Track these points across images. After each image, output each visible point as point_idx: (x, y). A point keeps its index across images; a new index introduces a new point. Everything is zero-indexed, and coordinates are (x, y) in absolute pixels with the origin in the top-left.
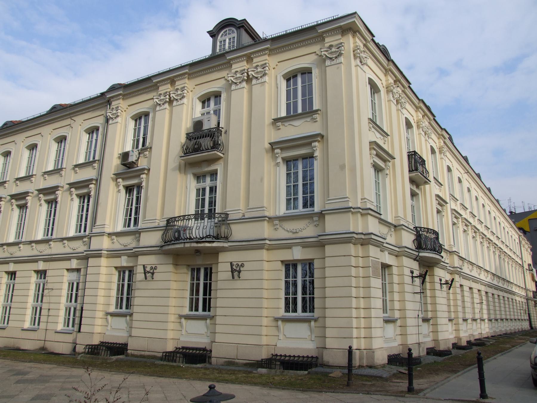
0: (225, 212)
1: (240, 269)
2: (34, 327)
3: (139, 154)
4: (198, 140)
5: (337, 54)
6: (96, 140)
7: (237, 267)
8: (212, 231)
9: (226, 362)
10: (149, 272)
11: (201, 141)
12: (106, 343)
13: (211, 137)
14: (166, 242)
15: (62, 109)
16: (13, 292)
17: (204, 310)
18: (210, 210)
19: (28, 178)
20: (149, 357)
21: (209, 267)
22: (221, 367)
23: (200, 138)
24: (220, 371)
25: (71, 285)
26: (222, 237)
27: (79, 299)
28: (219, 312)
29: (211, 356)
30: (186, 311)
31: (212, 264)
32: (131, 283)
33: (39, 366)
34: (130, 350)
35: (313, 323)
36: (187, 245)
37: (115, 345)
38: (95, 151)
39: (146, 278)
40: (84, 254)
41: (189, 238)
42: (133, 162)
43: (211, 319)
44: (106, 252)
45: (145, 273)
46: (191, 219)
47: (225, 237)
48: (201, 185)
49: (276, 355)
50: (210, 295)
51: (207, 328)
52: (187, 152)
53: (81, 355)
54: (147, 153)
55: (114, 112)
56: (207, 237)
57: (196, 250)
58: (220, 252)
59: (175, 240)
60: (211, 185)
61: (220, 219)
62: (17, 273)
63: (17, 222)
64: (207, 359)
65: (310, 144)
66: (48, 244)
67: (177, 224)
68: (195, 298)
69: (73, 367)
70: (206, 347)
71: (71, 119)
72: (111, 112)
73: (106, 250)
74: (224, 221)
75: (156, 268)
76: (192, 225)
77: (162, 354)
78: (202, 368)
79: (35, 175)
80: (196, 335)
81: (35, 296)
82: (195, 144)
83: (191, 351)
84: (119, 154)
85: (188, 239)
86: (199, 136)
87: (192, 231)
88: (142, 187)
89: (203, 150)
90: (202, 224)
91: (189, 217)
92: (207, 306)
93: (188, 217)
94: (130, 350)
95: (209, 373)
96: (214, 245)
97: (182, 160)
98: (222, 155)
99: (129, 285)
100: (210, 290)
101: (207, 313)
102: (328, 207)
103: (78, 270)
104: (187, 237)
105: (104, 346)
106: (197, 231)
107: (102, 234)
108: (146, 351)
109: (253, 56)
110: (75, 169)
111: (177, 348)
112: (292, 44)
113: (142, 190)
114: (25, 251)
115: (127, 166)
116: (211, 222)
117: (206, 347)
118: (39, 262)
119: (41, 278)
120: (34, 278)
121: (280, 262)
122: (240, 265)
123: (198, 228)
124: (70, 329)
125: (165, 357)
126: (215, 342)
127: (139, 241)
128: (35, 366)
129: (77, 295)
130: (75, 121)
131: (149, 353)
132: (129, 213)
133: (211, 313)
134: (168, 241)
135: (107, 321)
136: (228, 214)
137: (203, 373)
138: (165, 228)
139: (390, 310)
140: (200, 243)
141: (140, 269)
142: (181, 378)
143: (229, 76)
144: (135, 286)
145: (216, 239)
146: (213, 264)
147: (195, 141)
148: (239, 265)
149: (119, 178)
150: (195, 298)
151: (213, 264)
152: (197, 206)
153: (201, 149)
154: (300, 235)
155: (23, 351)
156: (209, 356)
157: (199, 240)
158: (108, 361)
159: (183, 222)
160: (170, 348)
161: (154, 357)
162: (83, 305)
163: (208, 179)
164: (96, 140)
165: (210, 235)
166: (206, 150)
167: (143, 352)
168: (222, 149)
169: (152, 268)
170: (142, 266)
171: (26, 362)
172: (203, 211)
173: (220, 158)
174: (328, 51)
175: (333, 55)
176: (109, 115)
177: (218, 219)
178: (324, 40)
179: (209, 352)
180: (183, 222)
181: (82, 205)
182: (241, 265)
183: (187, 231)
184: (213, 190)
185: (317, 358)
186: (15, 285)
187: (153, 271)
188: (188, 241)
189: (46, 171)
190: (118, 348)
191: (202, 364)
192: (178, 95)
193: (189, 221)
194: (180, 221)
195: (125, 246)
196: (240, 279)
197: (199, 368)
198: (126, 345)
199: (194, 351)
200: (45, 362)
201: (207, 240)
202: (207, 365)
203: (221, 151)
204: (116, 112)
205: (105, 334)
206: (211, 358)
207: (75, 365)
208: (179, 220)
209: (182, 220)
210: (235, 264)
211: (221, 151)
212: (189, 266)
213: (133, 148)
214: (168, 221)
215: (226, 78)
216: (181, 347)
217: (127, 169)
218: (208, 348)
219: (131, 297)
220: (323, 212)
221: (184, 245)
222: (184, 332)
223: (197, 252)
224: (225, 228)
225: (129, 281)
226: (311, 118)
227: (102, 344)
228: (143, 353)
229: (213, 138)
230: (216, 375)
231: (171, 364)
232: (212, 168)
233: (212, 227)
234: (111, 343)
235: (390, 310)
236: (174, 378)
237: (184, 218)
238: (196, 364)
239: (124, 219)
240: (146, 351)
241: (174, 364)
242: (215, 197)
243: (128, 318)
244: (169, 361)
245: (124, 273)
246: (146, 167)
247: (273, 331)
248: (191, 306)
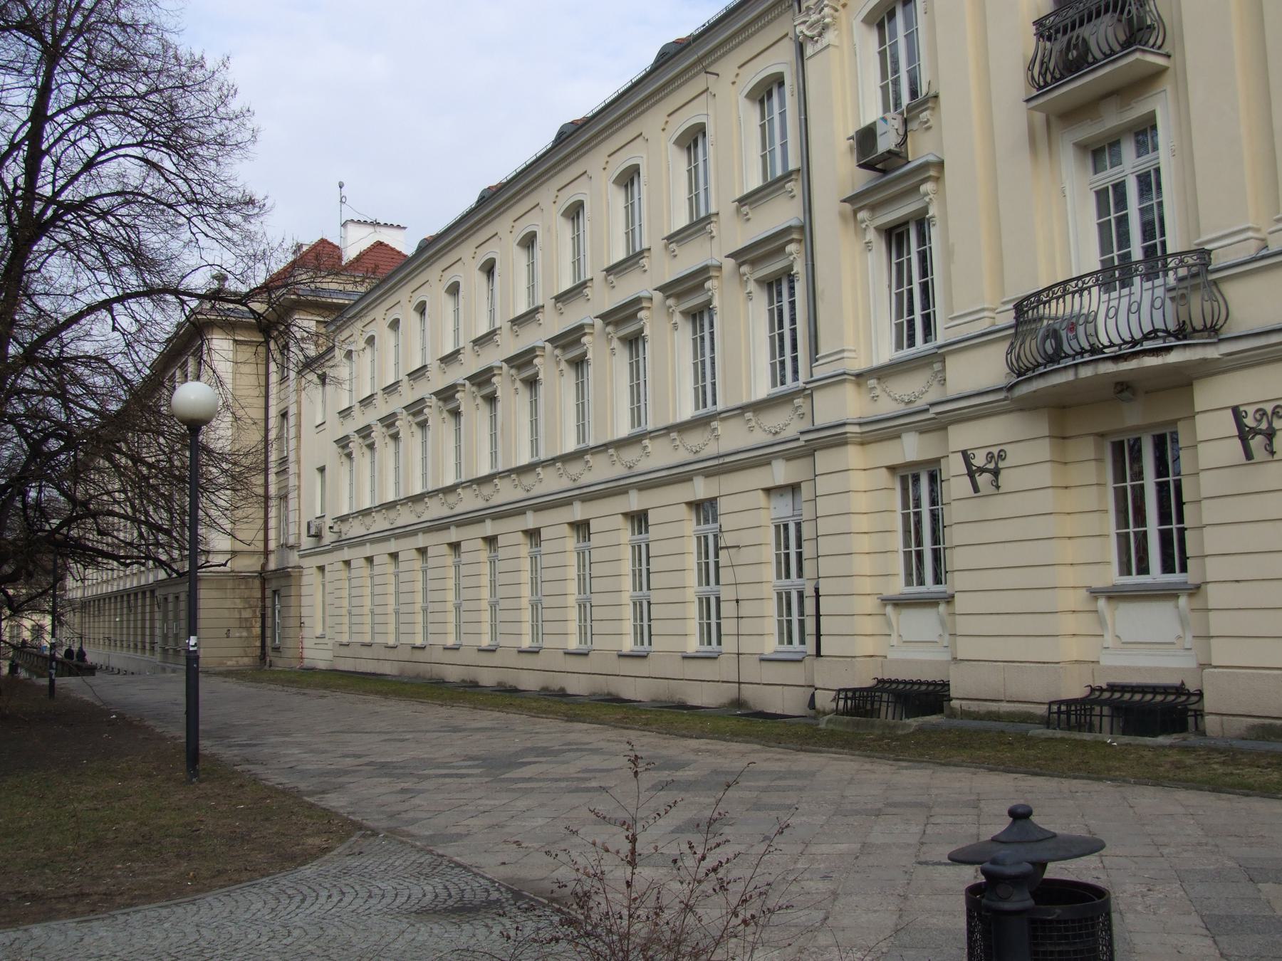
0: (1199, 244)
1: (1270, 423)
2: (709, 648)
3: (906, 122)
4: (1075, 34)
6: (783, 114)
7: (1260, 421)
8: (1158, 315)
9: (1253, 727)
10: (982, 470)
11: (1086, 31)
12: (891, 682)
13: (1115, 11)
14: (1022, 372)
15: (578, 129)
16: (648, 563)
17: (1167, 567)
18: (1149, 252)
19: (634, 259)
20: (1011, 717)
21: (1167, 431)
22: (1236, 744)
23: (1081, 24)
24: (1231, 754)
25: (781, 529)
26: (1195, 330)
27: (807, 565)
28: (1214, 569)
29: (1203, 710)
30: (1112, 576)
31: (1175, 422)
32: (940, 507)
33: (718, 747)
34: (958, 699)
36: (1085, 372)
37: (916, 687)
38: (784, 146)
39: (976, 489)
40: (801, 443)
41: (1088, 347)
42: (889, 152)
43: (1191, 595)
44: (857, 429)
45: (971, 475)
46: (1086, 289)
47: (1205, 329)
48: (1108, 177)
50: (1181, 519)
51: (1183, 622)
52: (1045, 81)
53: (827, 717)
54: (925, 115)
55: (814, 17)
56: (1146, 337)
57: (1117, 384)
58: (1197, 378)
59: (1048, 362)
60: (1143, 168)
61: (1182, 272)
62: (651, 514)
63: (629, 384)
64: (1191, 720)
66: (709, 429)
67: (1047, 311)
68: (1135, 533)
69: (801, 750)
70: (1183, 684)
71: (707, 72)
72: (804, 22)
73: (856, 421)
75: (1002, 456)
76: (1094, 307)
77: (1046, 706)
78: (1171, 747)
79: (718, 214)
80: (1151, 646)
81: (700, 570)
82: (1068, 48)
83: (1137, 697)
84: (849, 139)
85: (1087, 351)
86: (1077, 17)
87: (1096, 327)
88: (928, 219)
89: (1096, 61)
90: (1122, 300)
91: (1080, 284)
92: (1174, 556)
93: (1077, 285)
94: (958, 699)
95: (1193, 762)
96: (1173, 358)
97: (1034, 108)
98: (1161, 61)
99: (935, 517)
100: (1180, 504)
101: (1176, 577)
103: (794, 488)
104: (1082, 348)
105: (1102, 703)
106: (1111, 323)
107: (837, 380)
108: (1001, 701)
110: (742, 209)
111: (1093, 690)
113: (933, 230)
114: (659, 456)
115: (877, 166)
116: (1153, 288)
117: (1183, 684)
118: (695, 478)
119: (706, 521)
120: (690, 526)
121: (884, 470)
122: (1269, 412)
123: (1134, 308)
124: (798, 650)
125: (1059, 717)
127: (943, 381)
128: (709, 747)
129: (800, 555)
130: (718, 75)
131: (1012, 705)
132: (903, 304)
133: (1191, 577)
134: (1028, 369)
135: (889, 624)
136: (1209, 252)
137: (1172, 763)
138: (1012, 331)
139: (1109, 563)
140: (1126, 360)
141: (955, 466)
142: (1099, 779)
143: (796, 23)
144: (952, 514)
145: (1179, 339)
146: (1179, 420)
147: (1066, 37)
149: (861, 209)
150: (1135, 533)
151: (1179, 420)
152: (1105, 246)
153: (1090, 59)
155: (691, 712)
156: (1195, 711)
158: (900, 732)
159: (1064, 301)
160: (1075, 689)
161: (1027, 718)
162: (818, 583)
163: (1128, 150)
164: (783, 114)
165: (1155, 331)
166: (1106, 56)
167: (994, 704)
168: (1159, 42)
169: (993, 457)
170: (1230, 412)
171: (691, 737)
172: (1126, 257)
173: (1159, 72)
176: (802, 32)
177: (1176, 273)
179: (1194, 699)
180: (1064, 301)
181: (897, 264)
182: (1273, 413)
183: (1081, 329)
184: (1149, 183)
186: (651, 544)
187: (997, 464)
188: (1087, 358)
189: (745, 192)
190: (927, 694)
191: (1175, 736)
192: (811, 26)
193: (1081, 296)
194: (1054, 303)
195: (907, 403)
196: (1001, 491)
197: (1163, 747)
198: (946, 685)
199: (1149, 697)
200: (735, 736)
201: (1148, 345)
202: (1192, 739)
203: (1160, 48)
204: (819, 16)
206: (1202, 716)
207: (808, 744)
208: (1052, 299)
209: (1058, 298)
210: (1251, 410)
211: (1158, 49)
212: (1102, 435)
213: (886, 109)
214: (1019, 308)
216: (1104, 686)
217: (881, 177)
218: (1191, 686)
219: (945, 549)
221: (1076, 374)
222: (1109, 640)
223: (1122, 391)
224: (1203, 299)
225: (934, 502)
227: (880, 686)
228: (993, 707)
229: (1122, 12)
230: (1214, 769)
231: (1076, 735)
232: (1137, 111)
233: (1158, 303)
234: (905, 682)
235: (1109, 563)
236: (1075, 778)
237: (1064, 290)
238: (1155, 736)
239: (893, 326)
240: (1001, 701)
241: (1087, 736)
242: (1160, 204)
243: (942, 608)
244: (1069, 728)
245: (916, 479)
246: (931, 158)
247: (1084, 623)
248: (1125, 560)
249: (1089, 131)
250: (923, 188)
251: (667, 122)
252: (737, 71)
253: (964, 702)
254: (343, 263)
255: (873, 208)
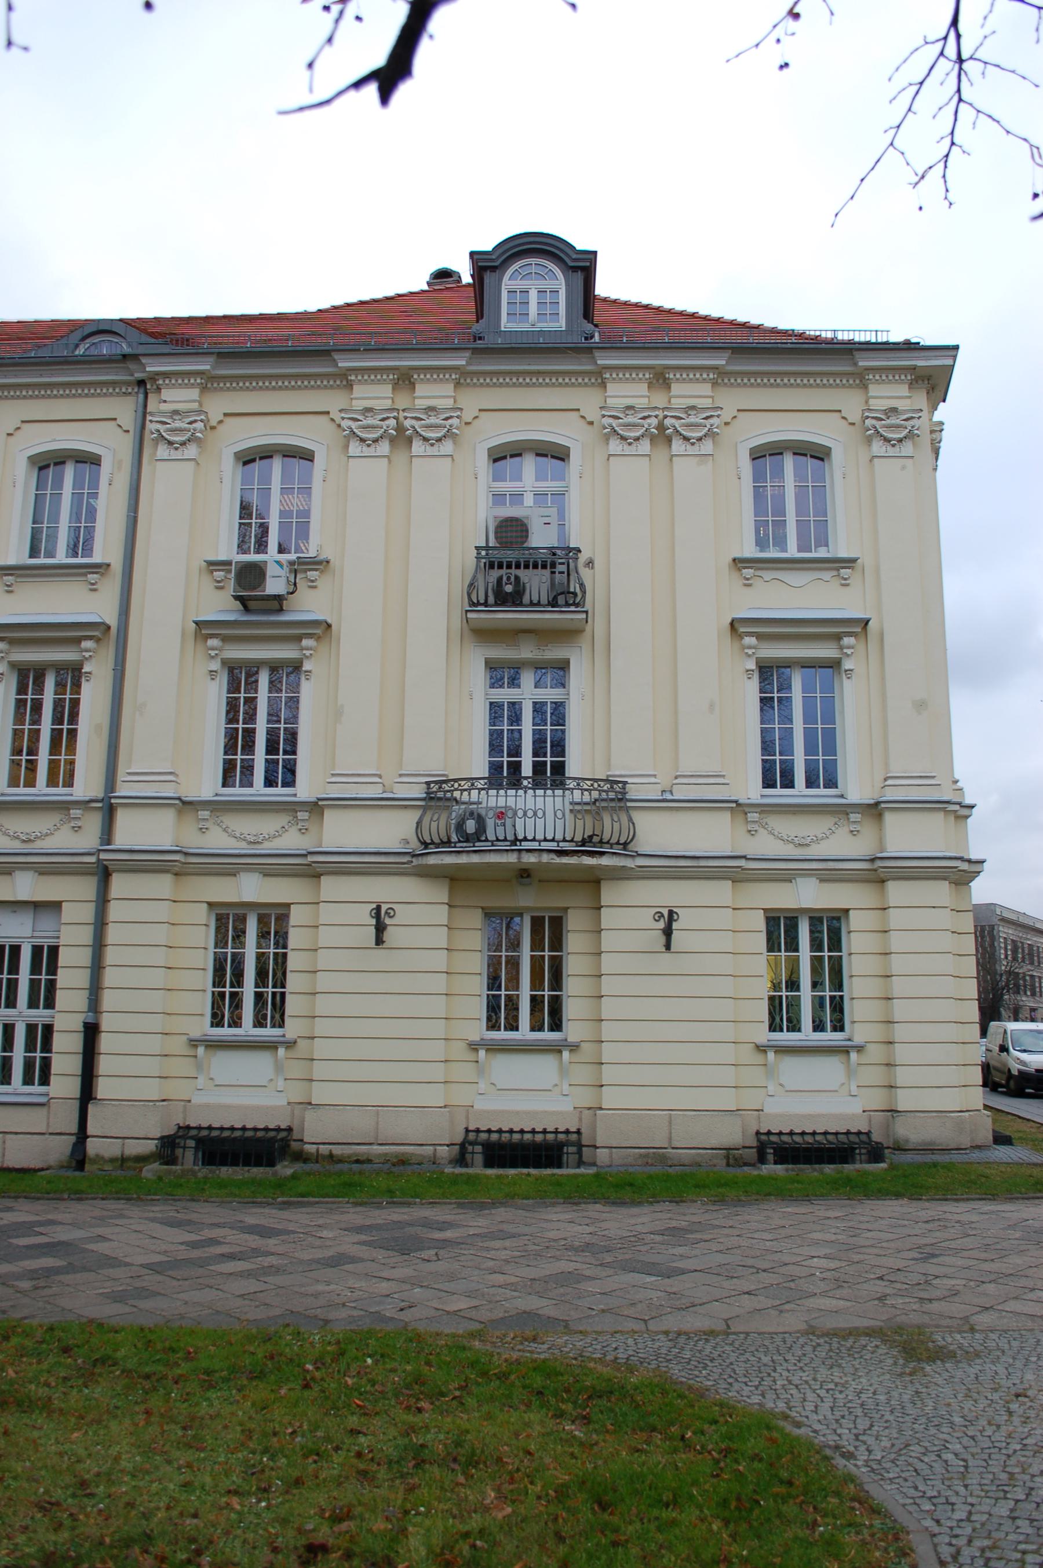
5: (905, 432)
8: (560, 823)
35: (281, 1051)
43: (287, 1048)
48: (505, 694)
49: (188, 1128)
65: (838, 637)
74: (620, 800)
102: (890, 795)
109: (353, 378)
111: (180, 1128)
112: (271, 377)
126: (601, 1109)
148: (663, 916)
154: (815, 851)
157: (493, 845)
174: (882, 420)
175: (369, 432)
178: (350, 386)
185: (290, 1130)
205: (189, 1101)
215: (331, 416)
220: (320, 803)
226: (835, 573)
247: (467, 1072)
249: (501, 652)
250: (305, 642)
251: (18, 428)
252: (735, 413)
253: (321, 1146)
254: (467, 278)
255: (225, 639)
